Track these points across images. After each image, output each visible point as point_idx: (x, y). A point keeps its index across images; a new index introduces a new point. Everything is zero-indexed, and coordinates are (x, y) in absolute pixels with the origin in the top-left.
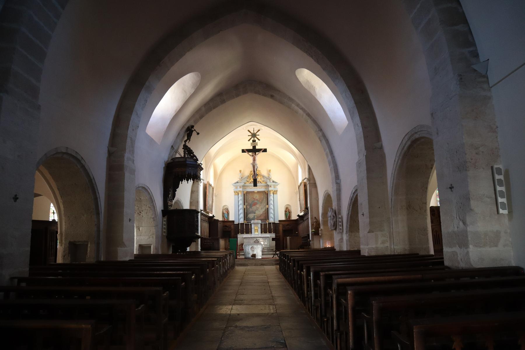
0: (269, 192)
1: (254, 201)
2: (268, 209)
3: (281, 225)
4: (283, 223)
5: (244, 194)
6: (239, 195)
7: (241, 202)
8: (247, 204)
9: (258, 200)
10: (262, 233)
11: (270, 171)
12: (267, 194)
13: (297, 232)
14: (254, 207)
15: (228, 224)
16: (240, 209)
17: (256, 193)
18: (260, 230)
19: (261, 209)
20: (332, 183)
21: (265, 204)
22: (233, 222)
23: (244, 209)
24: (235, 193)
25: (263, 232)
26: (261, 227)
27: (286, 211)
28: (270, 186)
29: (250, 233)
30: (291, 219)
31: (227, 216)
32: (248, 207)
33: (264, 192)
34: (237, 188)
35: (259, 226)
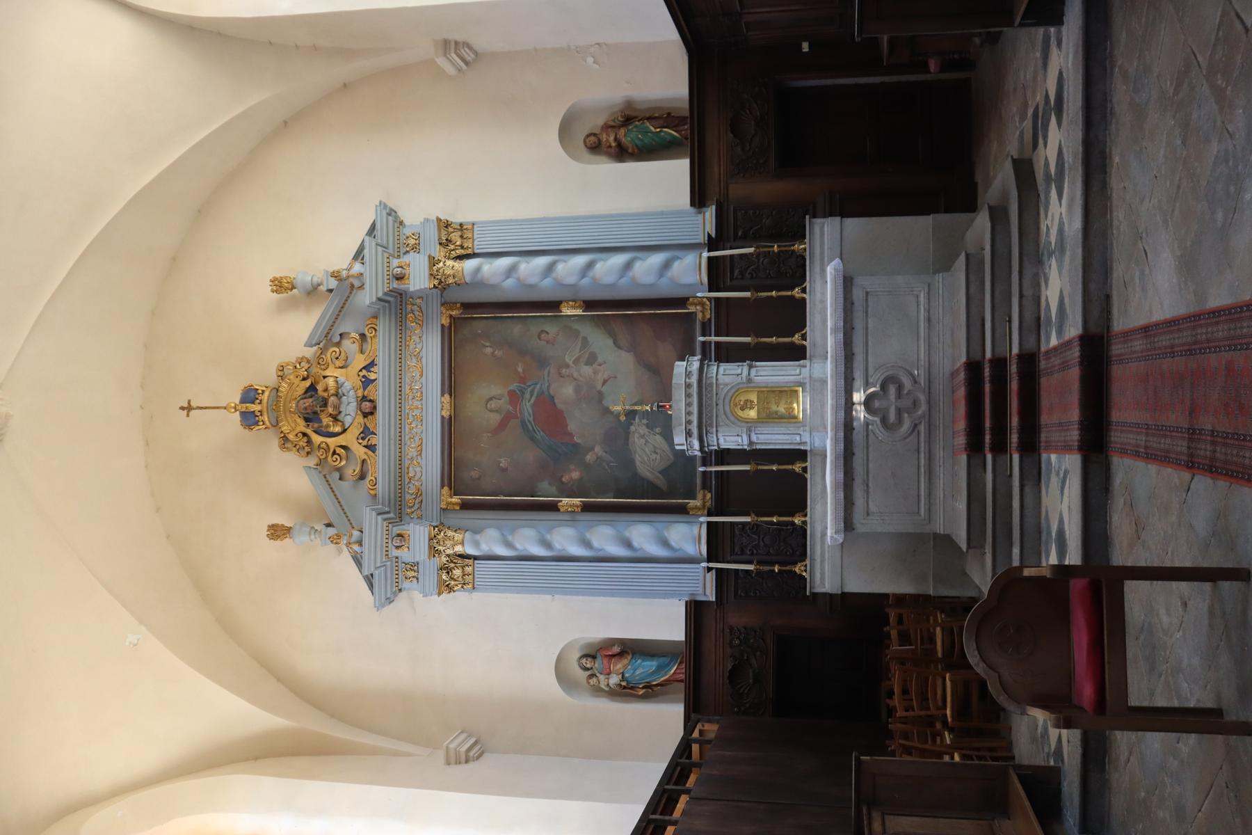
0: (453, 295)
1: (523, 424)
2: (589, 305)
3: (741, 189)
4: (716, 169)
5: (465, 506)
6: (471, 551)
7: (527, 538)
8: (544, 485)
9: (514, 386)
10: (798, 353)
11: (280, 285)
12: (467, 306)
13: (805, 47)
14: (572, 426)
15: (717, 662)
16: (587, 544)
17: (455, 407)
18: (770, 373)
19: (592, 360)
20: (854, 454)
21: (552, 329)
22: (695, 611)
23: (587, 508)
24: (450, 589)
25: (796, 338)
26: (741, 359)
27: (622, 153)
28: (400, 278)
29: (797, 467)
30: (687, 105)
31: (651, 665)
32: (575, 475)
33: (452, 337)
34: (414, 566)
35: (728, 374)
